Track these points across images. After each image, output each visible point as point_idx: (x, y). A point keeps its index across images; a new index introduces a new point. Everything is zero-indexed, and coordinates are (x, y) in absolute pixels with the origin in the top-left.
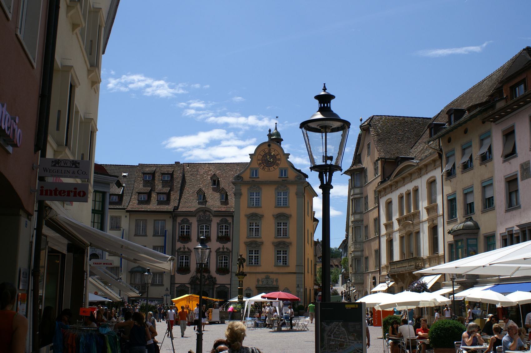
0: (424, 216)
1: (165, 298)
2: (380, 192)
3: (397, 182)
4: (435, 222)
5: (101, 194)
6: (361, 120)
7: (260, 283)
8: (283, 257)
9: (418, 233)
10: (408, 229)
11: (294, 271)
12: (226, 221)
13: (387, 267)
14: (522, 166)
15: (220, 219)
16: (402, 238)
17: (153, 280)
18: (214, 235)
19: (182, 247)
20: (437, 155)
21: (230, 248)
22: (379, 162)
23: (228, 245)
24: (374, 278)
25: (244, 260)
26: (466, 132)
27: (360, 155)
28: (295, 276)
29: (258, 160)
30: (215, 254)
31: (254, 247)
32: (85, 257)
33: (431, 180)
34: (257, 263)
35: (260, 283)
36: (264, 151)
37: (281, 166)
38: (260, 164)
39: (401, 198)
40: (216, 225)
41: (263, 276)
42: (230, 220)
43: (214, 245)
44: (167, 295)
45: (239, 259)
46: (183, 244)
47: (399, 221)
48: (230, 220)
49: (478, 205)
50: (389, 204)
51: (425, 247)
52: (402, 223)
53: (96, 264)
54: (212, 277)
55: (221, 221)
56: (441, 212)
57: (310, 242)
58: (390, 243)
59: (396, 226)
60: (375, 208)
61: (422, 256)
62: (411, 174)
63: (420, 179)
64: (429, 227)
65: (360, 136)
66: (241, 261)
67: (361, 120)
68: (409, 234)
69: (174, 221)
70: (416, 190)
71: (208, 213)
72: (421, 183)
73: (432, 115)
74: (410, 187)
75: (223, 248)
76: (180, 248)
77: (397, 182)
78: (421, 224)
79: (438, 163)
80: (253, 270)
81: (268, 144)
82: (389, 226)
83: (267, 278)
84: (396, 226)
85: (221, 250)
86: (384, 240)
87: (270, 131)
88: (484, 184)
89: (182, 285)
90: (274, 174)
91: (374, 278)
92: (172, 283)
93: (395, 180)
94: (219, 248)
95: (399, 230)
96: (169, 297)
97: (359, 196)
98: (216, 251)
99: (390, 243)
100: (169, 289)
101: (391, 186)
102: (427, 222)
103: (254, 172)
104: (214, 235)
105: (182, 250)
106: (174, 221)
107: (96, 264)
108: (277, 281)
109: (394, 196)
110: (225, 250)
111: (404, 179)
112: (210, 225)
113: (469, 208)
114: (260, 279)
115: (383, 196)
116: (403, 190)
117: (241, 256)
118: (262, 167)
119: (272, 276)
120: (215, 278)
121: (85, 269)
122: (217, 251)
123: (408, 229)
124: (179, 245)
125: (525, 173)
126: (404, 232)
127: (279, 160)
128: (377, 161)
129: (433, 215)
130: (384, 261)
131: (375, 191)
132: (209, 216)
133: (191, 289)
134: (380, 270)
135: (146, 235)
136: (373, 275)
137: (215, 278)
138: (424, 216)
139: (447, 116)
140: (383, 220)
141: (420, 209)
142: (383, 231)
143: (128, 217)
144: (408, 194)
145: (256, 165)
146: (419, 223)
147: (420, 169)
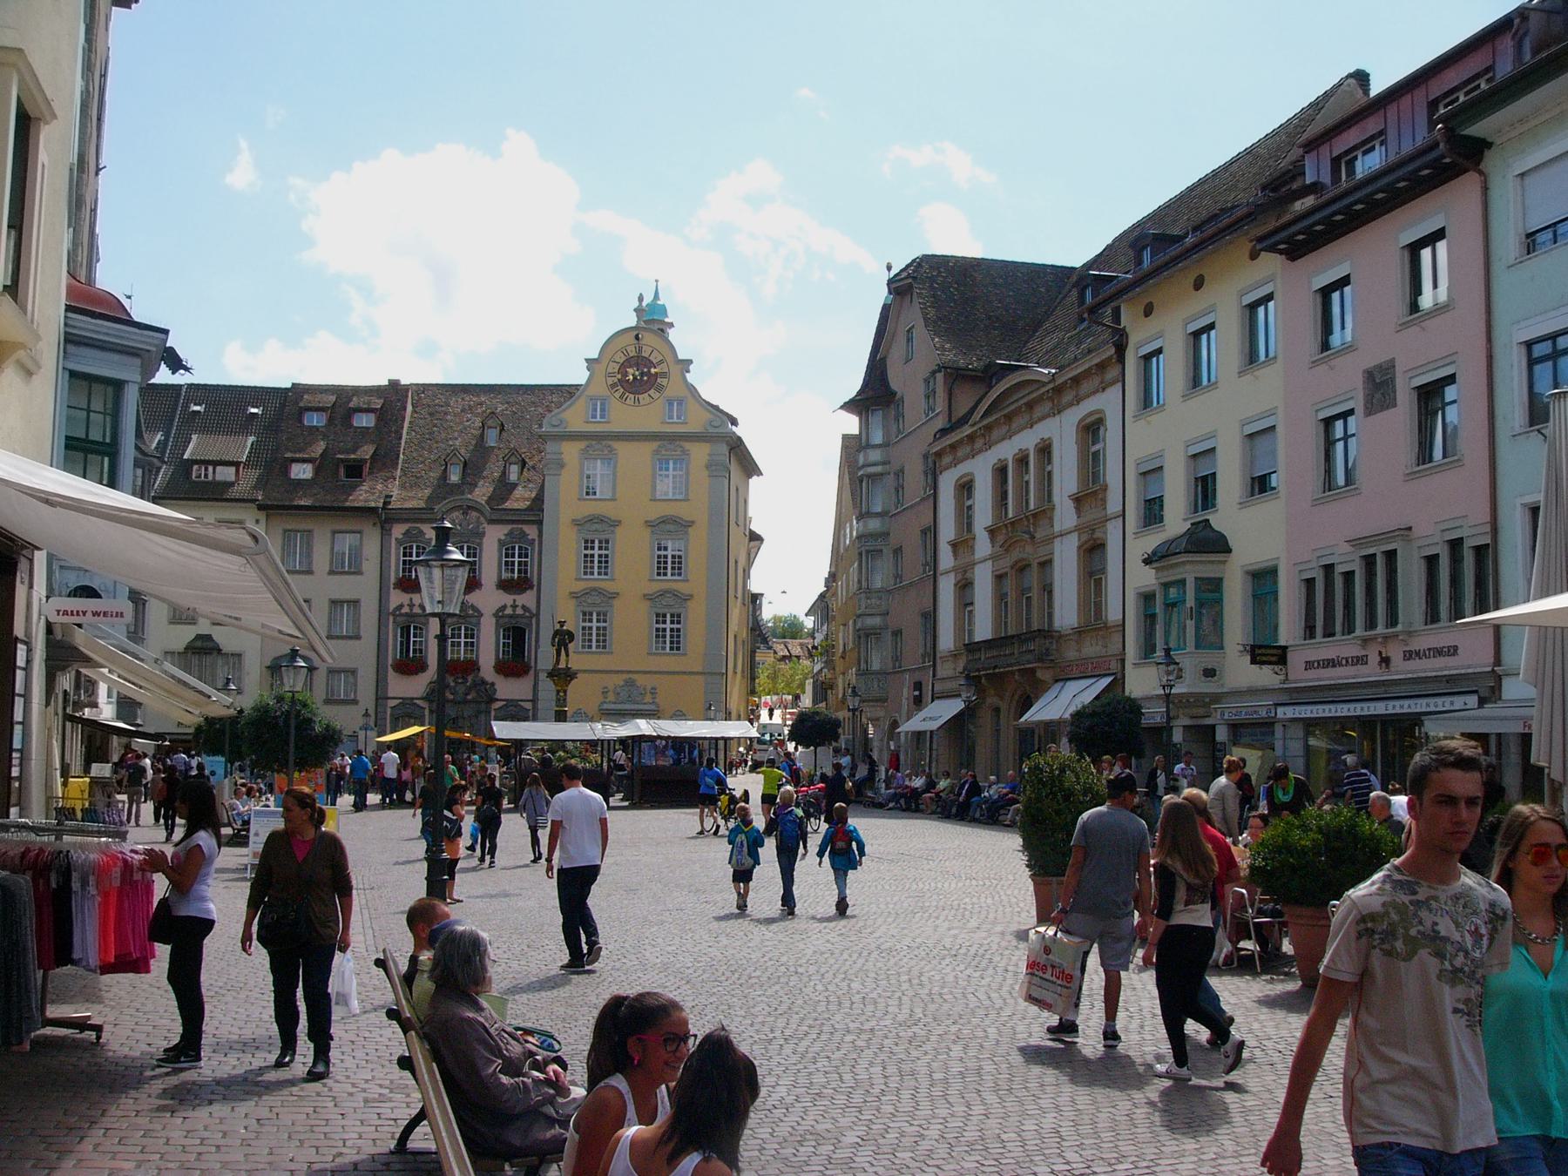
0: (1065, 515)
1: (361, 734)
2: (939, 454)
3: (989, 428)
4: (968, 575)
5: (110, 390)
6: (889, 268)
7: (611, 697)
8: (672, 630)
9: (1046, 564)
10: (1016, 555)
11: (700, 669)
12: (524, 534)
13: (955, 656)
14: (1369, 375)
15: (506, 529)
16: (999, 578)
17: (330, 690)
18: (490, 571)
19: (407, 602)
20: (1113, 351)
21: (532, 605)
22: (940, 376)
23: (527, 599)
24: (918, 686)
25: (571, 636)
26: (1199, 284)
27: (884, 359)
28: (701, 678)
29: (610, 375)
30: (494, 620)
31: (596, 604)
32: (20, 591)
33: (1089, 420)
34: (603, 643)
35: (611, 697)
36: (624, 351)
37: (668, 393)
38: (613, 386)
39: (1001, 471)
40: (496, 545)
41: (619, 680)
42: (531, 531)
43: (489, 599)
44: (365, 728)
45: (556, 633)
46: (407, 596)
47: (992, 532)
48: (531, 531)
49: (1230, 485)
50: (966, 488)
51: (1210, 567)
52: (1000, 539)
53: (66, 613)
54: (484, 682)
55: (510, 534)
56: (1113, 506)
57: (740, 595)
58: (965, 586)
59: (983, 546)
60: (923, 499)
61: (1057, 624)
62: (1030, 406)
63: (1057, 418)
64: (1079, 548)
65: (886, 309)
66: (563, 639)
67: (889, 268)
68: (1022, 568)
69: (385, 533)
70: (1045, 450)
71: (474, 514)
72: (1062, 430)
73: (1078, 264)
74: (1027, 440)
75: (514, 606)
76: (401, 606)
77: (989, 428)
78: (1057, 542)
79: (1113, 373)
80: (601, 662)
81: (636, 333)
82: (962, 544)
83: (630, 683)
84: (983, 546)
85: (509, 611)
86: (947, 587)
87: (641, 299)
88: (1249, 430)
89: (407, 702)
90: (644, 414)
91: (918, 686)
92: (381, 697)
93: (985, 422)
94: (505, 607)
95: (993, 558)
96: (374, 733)
97: (879, 469)
98: (495, 615)
99: (965, 586)
100: (372, 712)
101: (971, 438)
102: (952, 575)
103: (600, 406)
104: (490, 571)
105: (406, 610)
106: (385, 533)
107: (66, 613)
108: (654, 692)
109: (981, 468)
110: (519, 611)
111: (1008, 418)
112: (480, 544)
113: (1205, 490)
114: (611, 687)
115: (1071, 405)
116: (1006, 450)
117: (562, 624)
118: (617, 395)
119: (641, 680)
120: (493, 684)
121: (19, 630)
122: (499, 614)
123: (1016, 555)
124: (397, 598)
125: (1378, 396)
126: (1006, 563)
127: (664, 375)
128: (934, 373)
129: (1091, 515)
130: (947, 640)
131: (926, 457)
132: (479, 523)
133: (431, 712)
134: (934, 665)
135: (310, 572)
136: (917, 677)
137: (493, 684)
138: (1065, 515)
139: (1131, 253)
140: (947, 530)
141: (1056, 499)
142: (946, 559)
143: (274, 549)
144: (1022, 460)
145: (601, 389)
146: (1050, 540)
147: (1059, 390)
